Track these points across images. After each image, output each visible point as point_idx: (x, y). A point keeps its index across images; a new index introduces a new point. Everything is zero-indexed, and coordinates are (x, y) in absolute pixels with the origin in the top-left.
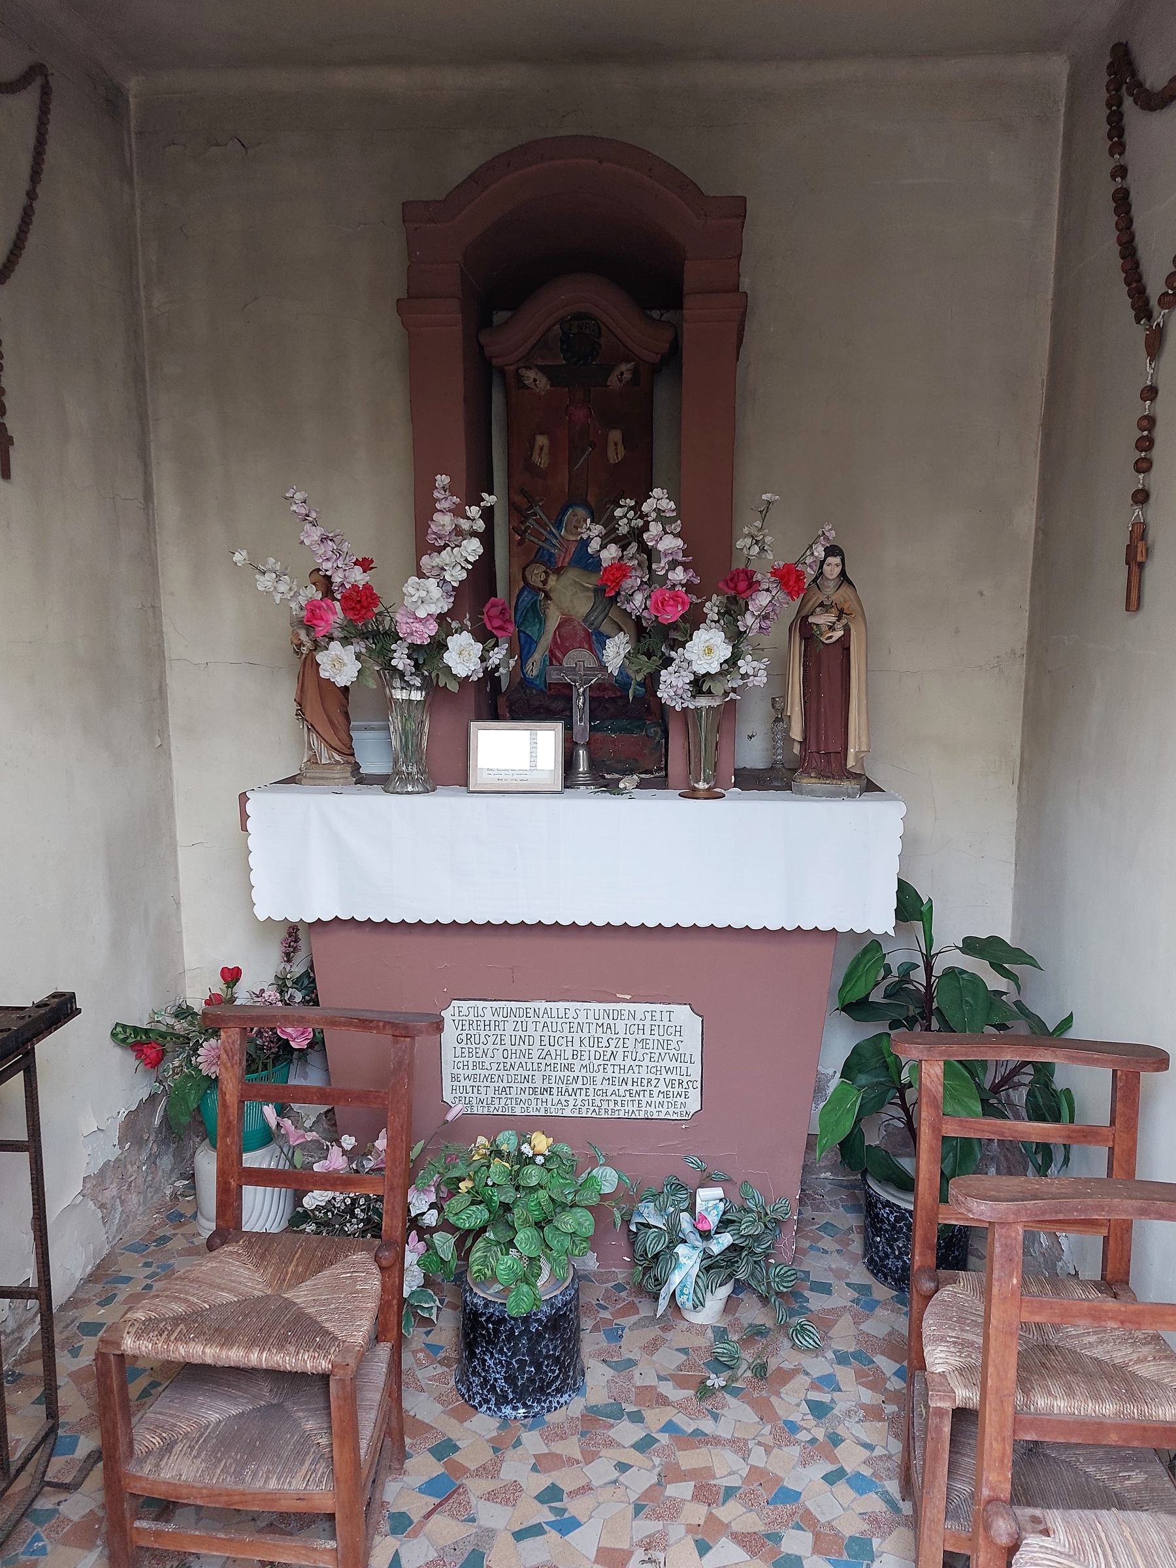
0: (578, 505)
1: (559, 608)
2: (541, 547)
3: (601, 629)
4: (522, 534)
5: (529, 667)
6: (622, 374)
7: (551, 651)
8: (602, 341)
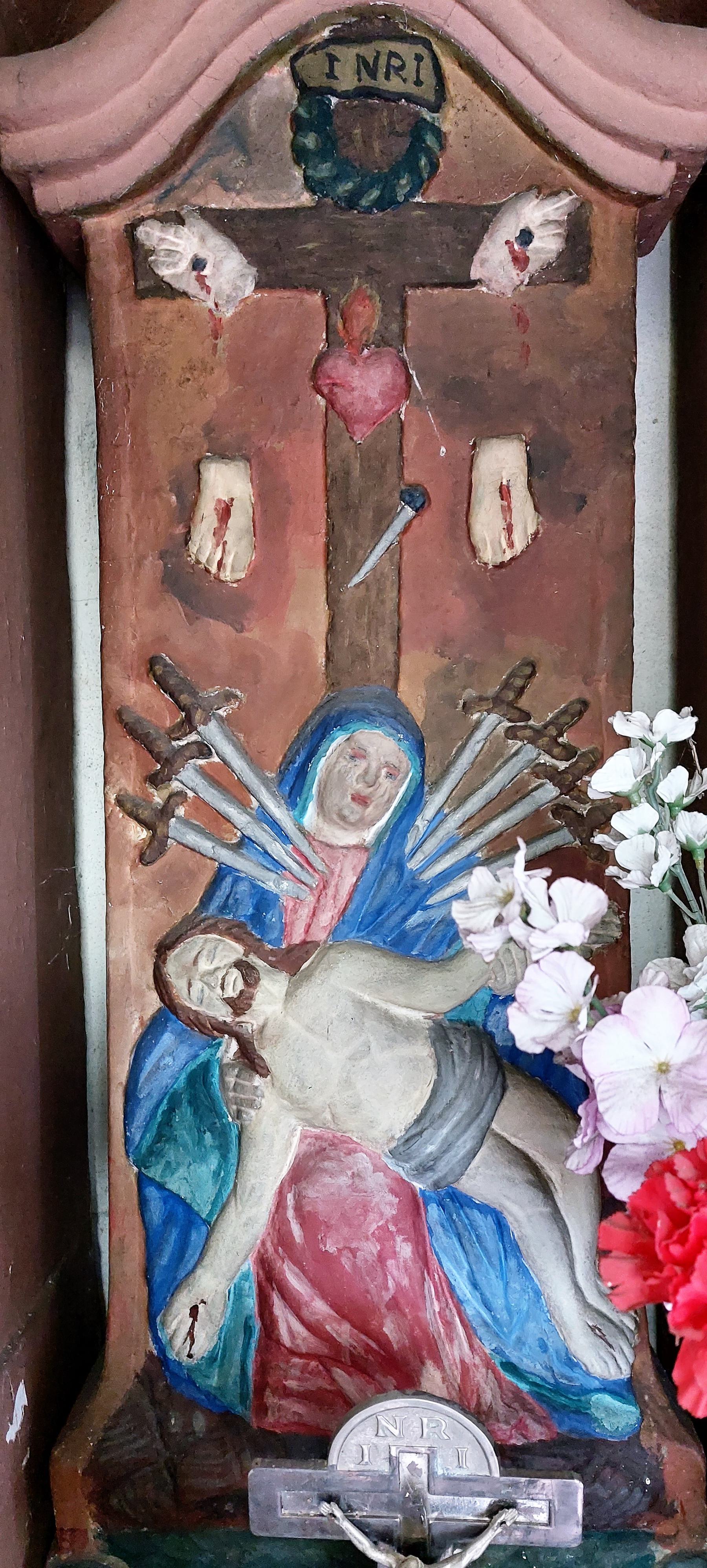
0: (366, 716)
1: (296, 1104)
2: (222, 873)
3: (468, 1185)
4: (155, 821)
5: (177, 1321)
6: (526, 236)
7: (264, 1263)
8: (448, 121)
